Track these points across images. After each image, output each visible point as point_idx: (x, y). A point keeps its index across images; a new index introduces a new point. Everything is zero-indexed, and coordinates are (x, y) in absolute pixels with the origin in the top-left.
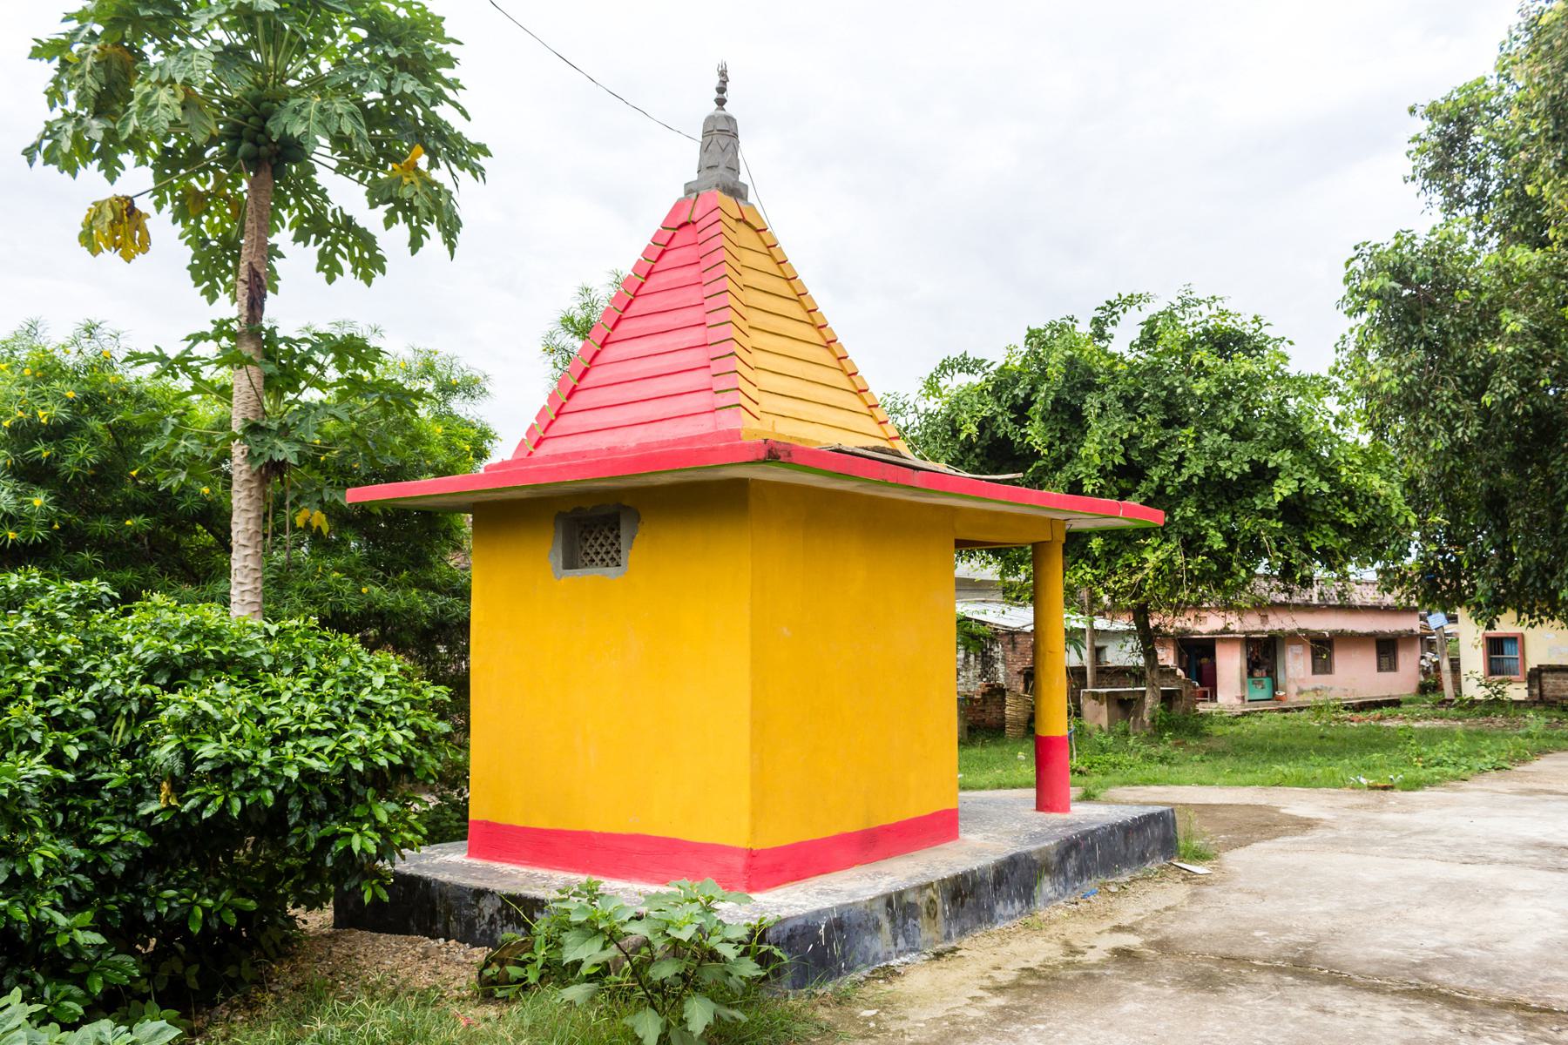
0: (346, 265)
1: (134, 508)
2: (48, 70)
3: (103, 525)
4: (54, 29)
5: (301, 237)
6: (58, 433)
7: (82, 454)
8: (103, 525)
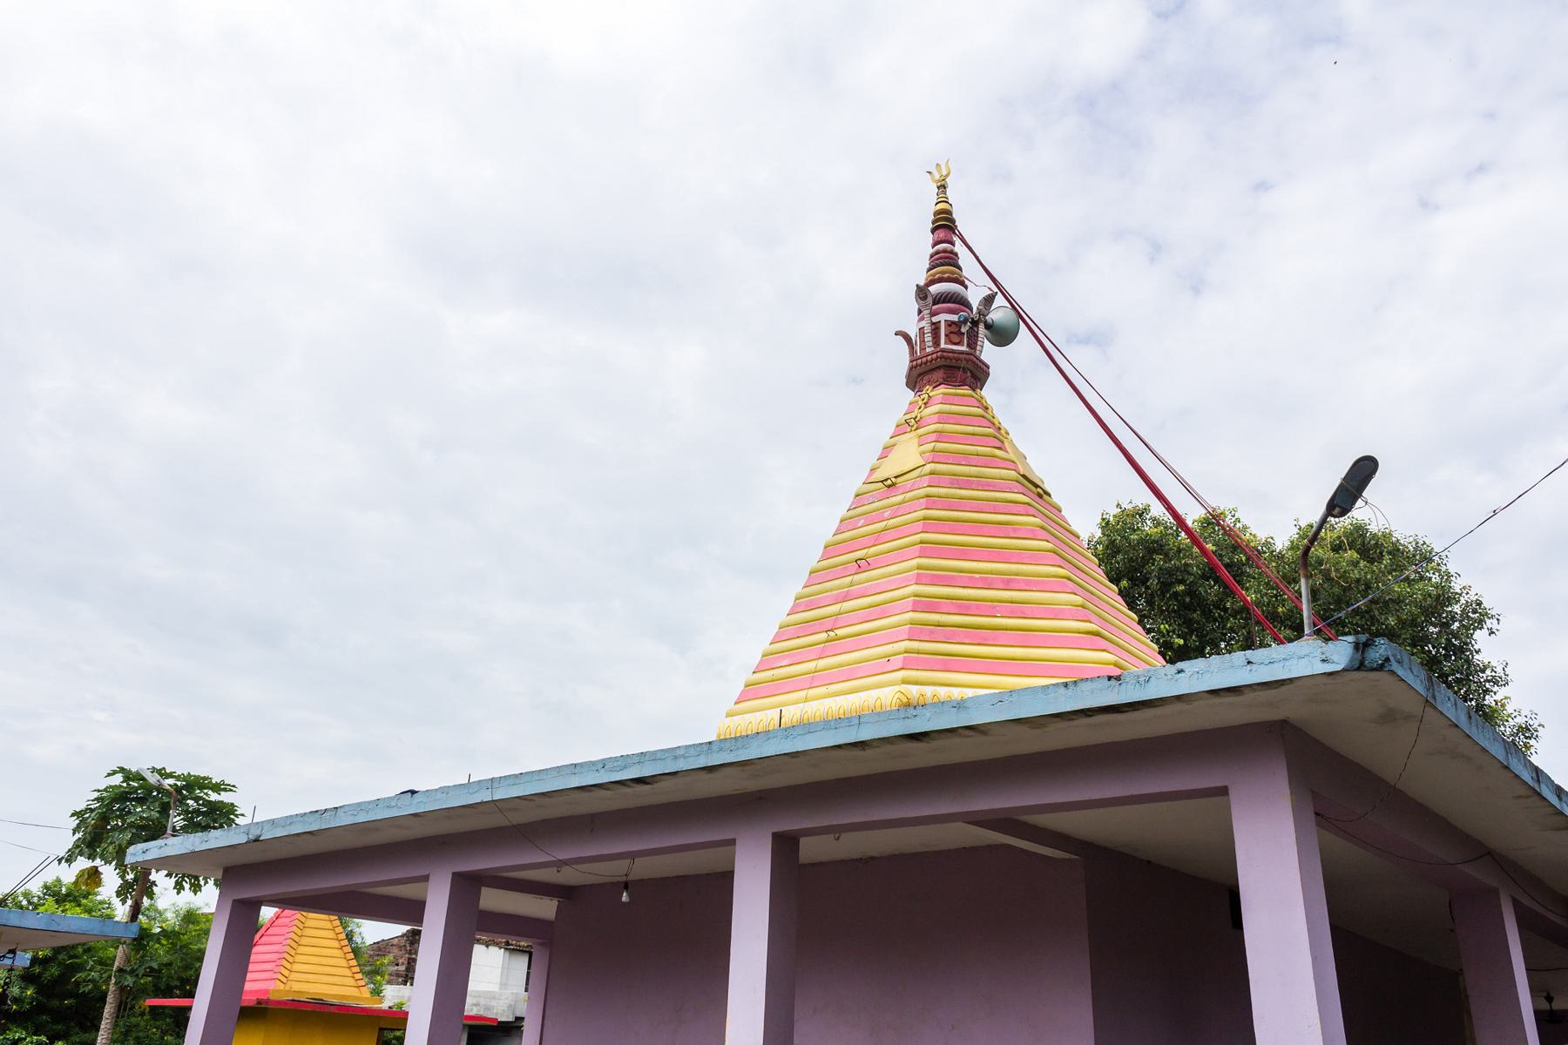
0: (187, 886)
1: (70, 995)
2: (74, 822)
3: (55, 1003)
4: (81, 806)
5: (169, 875)
6: (45, 962)
7: (54, 971)
8: (55, 1003)
